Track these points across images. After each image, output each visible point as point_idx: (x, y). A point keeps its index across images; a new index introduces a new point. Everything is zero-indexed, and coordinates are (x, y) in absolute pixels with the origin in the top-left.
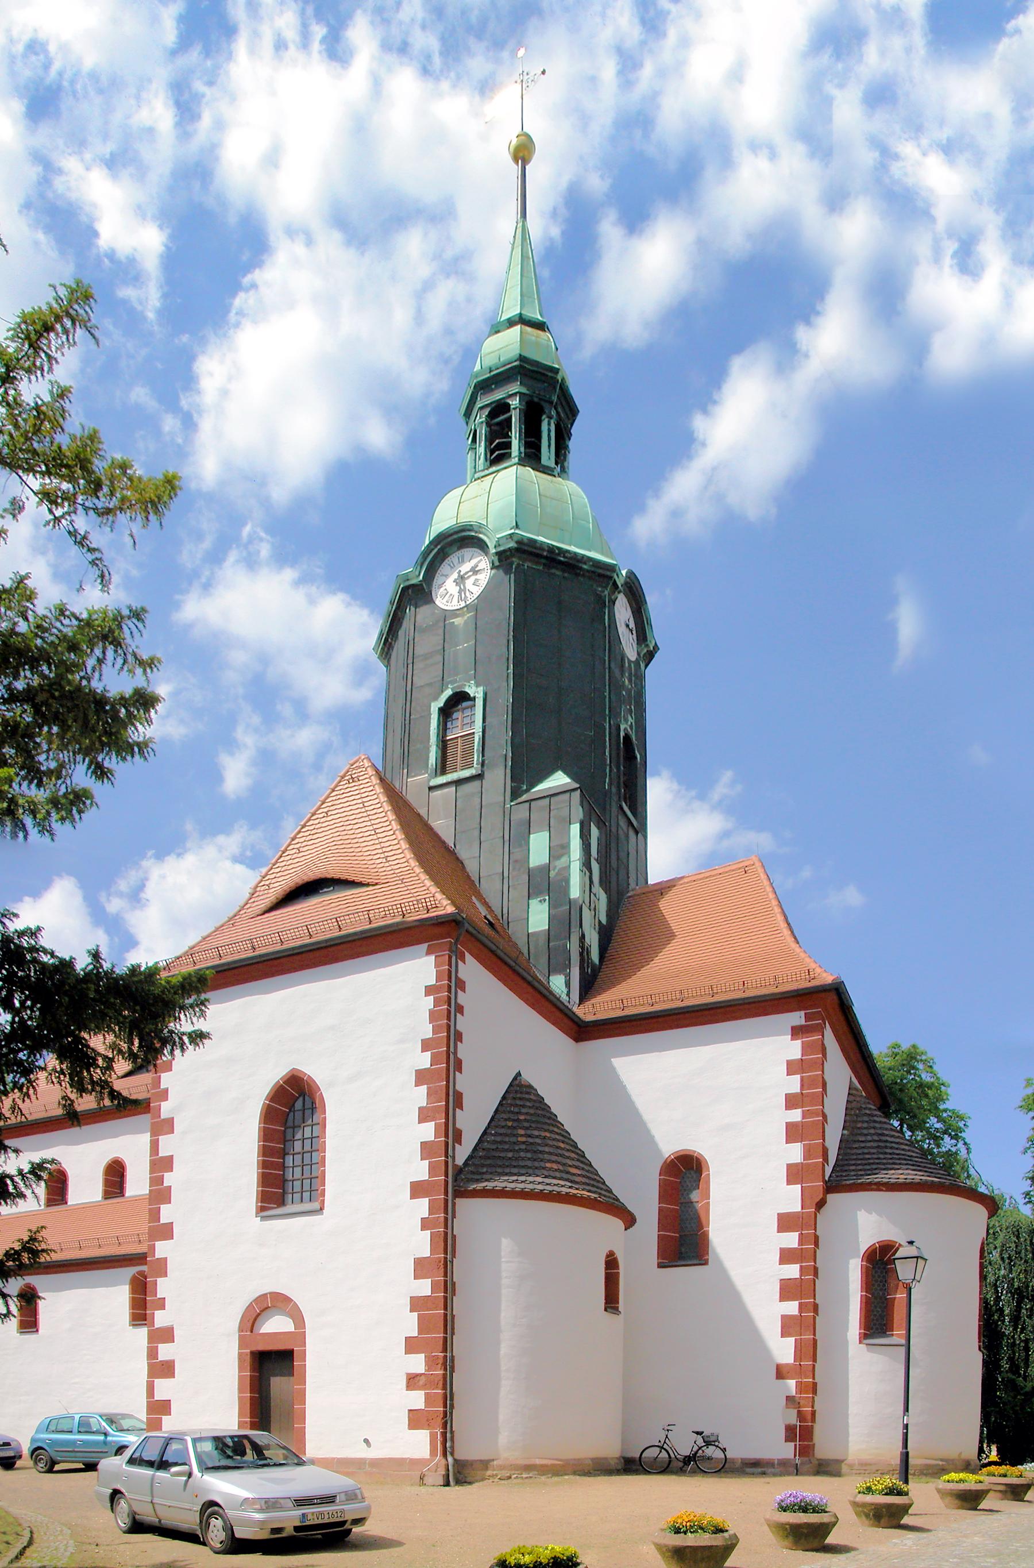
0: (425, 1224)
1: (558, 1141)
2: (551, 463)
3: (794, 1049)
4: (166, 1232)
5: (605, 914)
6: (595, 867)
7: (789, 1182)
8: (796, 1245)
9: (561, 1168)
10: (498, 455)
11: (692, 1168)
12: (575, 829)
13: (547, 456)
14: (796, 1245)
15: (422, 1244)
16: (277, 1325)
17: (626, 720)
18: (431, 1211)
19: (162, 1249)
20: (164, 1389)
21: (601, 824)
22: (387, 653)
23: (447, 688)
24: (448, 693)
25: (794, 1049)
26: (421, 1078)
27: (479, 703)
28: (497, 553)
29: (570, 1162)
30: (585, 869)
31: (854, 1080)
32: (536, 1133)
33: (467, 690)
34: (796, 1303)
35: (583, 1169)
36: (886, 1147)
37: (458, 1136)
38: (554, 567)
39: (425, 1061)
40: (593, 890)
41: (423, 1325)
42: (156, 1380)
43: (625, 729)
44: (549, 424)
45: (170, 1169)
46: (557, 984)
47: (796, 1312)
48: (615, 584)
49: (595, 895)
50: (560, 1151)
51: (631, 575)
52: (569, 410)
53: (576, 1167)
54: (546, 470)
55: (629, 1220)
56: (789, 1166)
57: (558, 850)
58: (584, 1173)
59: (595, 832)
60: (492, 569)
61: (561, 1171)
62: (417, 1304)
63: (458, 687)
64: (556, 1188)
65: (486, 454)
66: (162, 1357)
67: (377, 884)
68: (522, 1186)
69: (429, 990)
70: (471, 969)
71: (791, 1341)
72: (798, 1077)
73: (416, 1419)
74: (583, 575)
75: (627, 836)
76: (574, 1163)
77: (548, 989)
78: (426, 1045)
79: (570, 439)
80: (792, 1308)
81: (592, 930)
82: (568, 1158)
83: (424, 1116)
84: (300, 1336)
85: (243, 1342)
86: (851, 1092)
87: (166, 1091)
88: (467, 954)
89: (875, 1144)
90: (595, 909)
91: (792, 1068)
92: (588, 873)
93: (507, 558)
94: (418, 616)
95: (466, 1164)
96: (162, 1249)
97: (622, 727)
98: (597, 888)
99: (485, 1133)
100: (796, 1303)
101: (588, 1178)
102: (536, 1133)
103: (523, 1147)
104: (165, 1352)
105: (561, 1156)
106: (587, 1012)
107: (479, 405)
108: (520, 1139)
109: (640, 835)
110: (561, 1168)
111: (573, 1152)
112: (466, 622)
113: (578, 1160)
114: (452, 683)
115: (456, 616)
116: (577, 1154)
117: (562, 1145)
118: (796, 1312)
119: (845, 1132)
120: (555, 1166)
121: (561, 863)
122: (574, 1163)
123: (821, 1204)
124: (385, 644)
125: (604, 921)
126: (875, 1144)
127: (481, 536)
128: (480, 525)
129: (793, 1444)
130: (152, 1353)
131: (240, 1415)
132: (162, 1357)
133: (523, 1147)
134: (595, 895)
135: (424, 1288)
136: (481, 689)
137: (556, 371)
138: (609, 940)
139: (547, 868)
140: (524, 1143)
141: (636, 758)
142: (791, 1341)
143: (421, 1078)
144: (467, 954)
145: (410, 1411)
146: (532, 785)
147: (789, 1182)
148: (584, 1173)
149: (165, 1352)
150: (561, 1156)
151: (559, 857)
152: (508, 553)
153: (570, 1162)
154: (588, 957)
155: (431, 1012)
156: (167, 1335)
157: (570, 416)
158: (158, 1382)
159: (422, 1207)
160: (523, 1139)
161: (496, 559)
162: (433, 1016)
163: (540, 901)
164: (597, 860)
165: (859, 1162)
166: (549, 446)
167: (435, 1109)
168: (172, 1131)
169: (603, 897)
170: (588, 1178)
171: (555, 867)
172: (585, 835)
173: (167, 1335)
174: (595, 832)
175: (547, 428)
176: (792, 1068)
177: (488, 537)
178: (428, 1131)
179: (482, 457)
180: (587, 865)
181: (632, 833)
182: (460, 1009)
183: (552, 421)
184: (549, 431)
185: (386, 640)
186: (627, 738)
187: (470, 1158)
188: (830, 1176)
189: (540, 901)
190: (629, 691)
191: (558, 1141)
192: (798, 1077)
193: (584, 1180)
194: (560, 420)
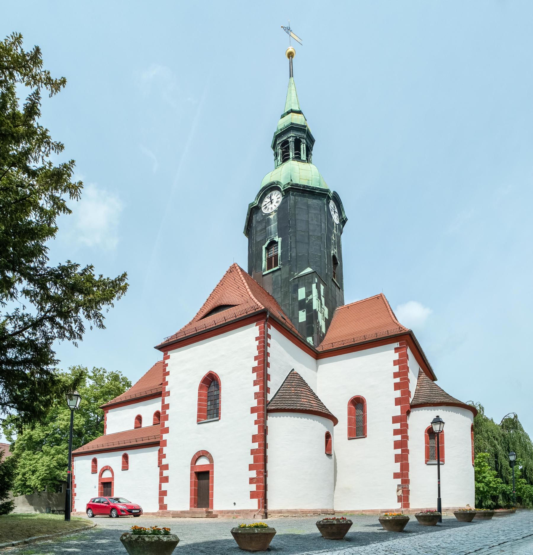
0: (256, 422)
1: (307, 392)
2: (305, 159)
3: (396, 356)
4: (167, 431)
5: (327, 315)
6: (323, 299)
7: (396, 405)
8: (399, 428)
9: (308, 401)
10: (285, 159)
11: (360, 402)
12: (314, 286)
13: (303, 157)
14: (399, 428)
15: (255, 430)
16: (203, 462)
17: (334, 251)
18: (258, 417)
19: (165, 436)
20: (165, 486)
21: (324, 284)
22: (248, 233)
23: (268, 240)
24: (269, 241)
25: (396, 356)
26: (254, 370)
27: (280, 244)
28: (284, 191)
29: (311, 399)
30: (318, 299)
31: (421, 369)
32: (299, 389)
33: (275, 239)
34: (400, 436)
35: (316, 401)
36: (433, 391)
37: (268, 390)
38: (305, 193)
39: (256, 364)
40: (322, 307)
41: (255, 460)
42: (162, 484)
43: (333, 253)
44: (303, 146)
45: (168, 408)
46: (310, 340)
47: (400, 453)
48: (329, 196)
49: (323, 308)
50: (307, 395)
51: (335, 193)
52: (311, 140)
53: (314, 401)
54: (303, 161)
55: (335, 421)
56: (396, 399)
57: (309, 293)
58: (317, 403)
59: (322, 287)
60: (282, 196)
61: (308, 402)
62: (253, 452)
63: (272, 239)
64: (305, 408)
65: (281, 159)
66: (164, 475)
67: (238, 305)
68: (292, 407)
69: (257, 339)
70: (272, 331)
71: (399, 464)
72: (398, 366)
73: (253, 495)
74: (316, 195)
75: (335, 290)
76: (313, 399)
77: (306, 342)
78: (256, 358)
79: (312, 151)
80: (399, 451)
81: (322, 320)
82: (310, 397)
83: (255, 383)
84: (212, 466)
85: (192, 469)
86: (420, 373)
87: (167, 382)
88: (271, 326)
89: (429, 390)
90: (323, 313)
91: (395, 363)
92: (320, 301)
93: (288, 192)
94: (257, 218)
95: (271, 400)
96: (165, 436)
97: (332, 252)
98: (324, 306)
99: (279, 390)
100: (400, 436)
101: (318, 404)
102: (299, 389)
103: (293, 394)
104: (165, 473)
105: (308, 397)
106: (319, 349)
107: (278, 143)
108: (292, 391)
109: (340, 289)
110: (308, 401)
111: (313, 396)
112: (274, 217)
113: (314, 398)
114: (269, 238)
115: (270, 215)
116: (315, 397)
117: (308, 393)
118: (400, 453)
119: (418, 387)
120: (305, 400)
121: (309, 298)
122: (313, 399)
123: (408, 413)
124: (247, 230)
125: (327, 318)
126: (429, 390)
127: (278, 186)
128: (278, 182)
129: (401, 503)
130: (161, 474)
131: (191, 495)
132: (164, 475)
133: (293, 394)
134: (323, 308)
135: (256, 446)
136: (280, 239)
137: (305, 126)
138: (329, 324)
139: (304, 300)
140: (293, 392)
141: (338, 263)
142: (399, 464)
143: (254, 370)
144: (271, 326)
145: (250, 492)
146: (299, 273)
147: (396, 405)
148: (317, 403)
149: (165, 473)
150: (308, 397)
151: (309, 296)
152: (288, 190)
153: (311, 399)
154: (321, 331)
155: (258, 346)
156: (166, 467)
157: (312, 143)
158: (163, 484)
159: (255, 416)
160: (294, 391)
161: (284, 193)
162: (258, 348)
163: (303, 311)
164: (323, 297)
165: (423, 397)
166: (304, 153)
167: (259, 381)
168: (169, 395)
169: (326, 310)
170: (318, 404)
171: (308, 299)
172: (318, 288)
173: (166, 467)
174: (322, 287)
175: (303, 147)
176: (395, 363)
177: (281, 186)
178: (257, 389)
179: (280, 160)
180: (319, 298)
181: (337, 289)
182: (268, 345)
183: (304, 144)
184: (304, 148)
185: (247, 228)
186: (334, 256)
187: (273, 398)
188: (412, 402)
189: (303, 311)
190: (335, 241)
191: (307, 392)
192: (398, 366)
193: (316, 405)
194: (308, 143)
